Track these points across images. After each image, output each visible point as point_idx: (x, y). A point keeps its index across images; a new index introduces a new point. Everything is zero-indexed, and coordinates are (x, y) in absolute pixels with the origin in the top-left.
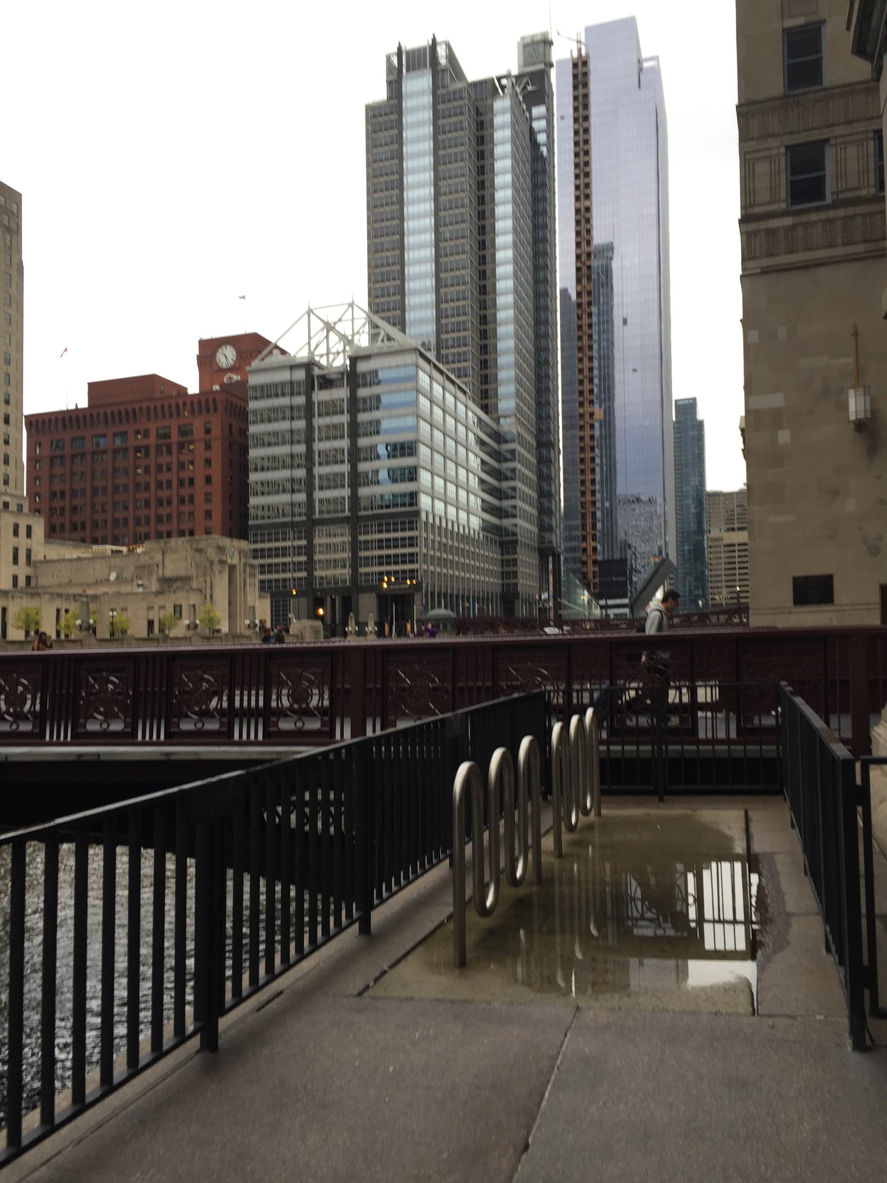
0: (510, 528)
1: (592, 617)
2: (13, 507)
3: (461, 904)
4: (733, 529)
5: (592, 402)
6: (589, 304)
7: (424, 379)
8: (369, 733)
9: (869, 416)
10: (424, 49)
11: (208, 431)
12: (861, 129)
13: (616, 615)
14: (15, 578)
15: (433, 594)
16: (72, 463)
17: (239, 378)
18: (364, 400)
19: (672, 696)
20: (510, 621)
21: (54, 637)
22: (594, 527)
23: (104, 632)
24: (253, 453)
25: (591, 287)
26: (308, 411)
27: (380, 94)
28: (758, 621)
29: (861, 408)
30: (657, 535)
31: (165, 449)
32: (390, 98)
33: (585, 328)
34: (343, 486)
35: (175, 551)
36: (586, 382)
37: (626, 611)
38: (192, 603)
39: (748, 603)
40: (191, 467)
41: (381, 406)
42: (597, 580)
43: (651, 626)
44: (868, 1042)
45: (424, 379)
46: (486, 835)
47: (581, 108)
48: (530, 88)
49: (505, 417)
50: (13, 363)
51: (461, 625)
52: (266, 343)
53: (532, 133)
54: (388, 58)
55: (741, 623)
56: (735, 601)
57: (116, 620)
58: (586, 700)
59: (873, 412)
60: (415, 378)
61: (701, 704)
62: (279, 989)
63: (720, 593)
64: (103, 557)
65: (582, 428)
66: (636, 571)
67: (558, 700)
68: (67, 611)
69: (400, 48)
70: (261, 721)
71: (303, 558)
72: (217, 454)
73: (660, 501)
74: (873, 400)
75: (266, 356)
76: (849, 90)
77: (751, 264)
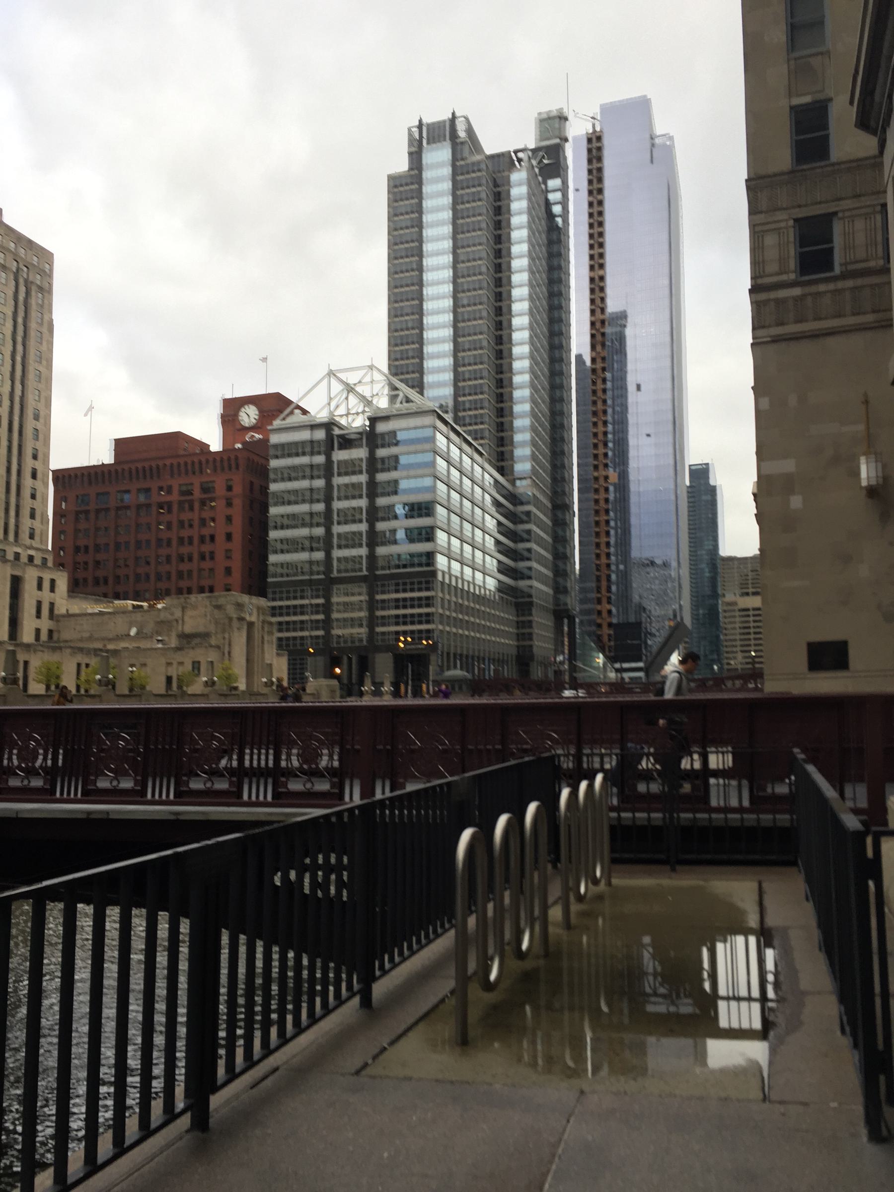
0: (526, 590)
1: (608, 681)
2: (38, 561)
3: (463, 979)
4: (747, 594)
5: (606, 466)
6: (604, 369)
7: (441, 441)
8: (379, 796)
9: (881, 481)
10: (444, 122)
11: (229, 488)
12: (868, 203)
13: (631, 678)
14: (38, 631)
15: (448, 654)
16: (97, 518)
17: (261, 437)
18: (383, 460)
19: (685, 764)
20: (526, 683)
21: (74, 691)
22: (609, 590)
23: (123, 688)
24: (274, 511)
25: (604, 354)
26: (328, 470)
27: (402, 165)
28: (772, 687)
29: (873, 474)
30: (671, 599)
31: (187, 506)
32: (411, 169)
33: (600, 393)
34: (361, 545)
35: (195, 607)
36: (601, 446)
37: (641, 674)
38: (210, 660)
39: (762, 668)
40: (212, 524)
41: (399, 467)
42: (612, 643)
43: (670, 688)
44: (885, 1132)
45: (441, 441)
46: (490, 906)
47: (595, 181)
48: (546, 161)
49: (520, 479)
50: (42, 420)
51: (476, 687)
52: (288, 402)
53: (548, 204)
54: (409, 130)
55: (756, 689)
56: (750, 666)
57: (135, 675)
58: (597, 766)
59: (885, 478)
60: (433, 439)
61: (714, 771)
62: (275, 1065)
63: (735, 658)
64: (124, 612)
65: (596, 491)
66: (650, 634)
67: (568, 764)
68: (87, 665)
69: (420, 121)
70: (270, 781)
71: (321, 617)
72: (238, 511)
73: (674, 564)
74: (884, 467)
75: (288, 415)
76: (857, 165)
77: (761, 332)
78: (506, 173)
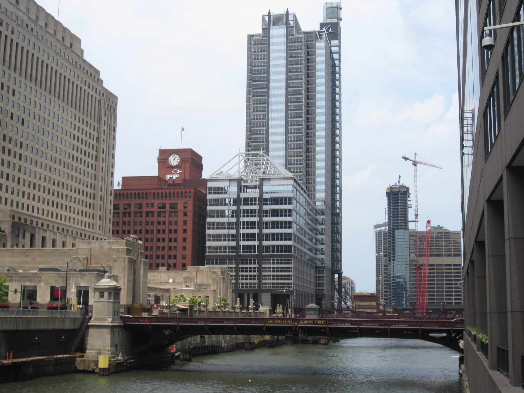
48: (330, 31)
53: (331, 53)
54: (263, 16)
69: (269, 13)
72: (190, 218)
78: (313, 42)
